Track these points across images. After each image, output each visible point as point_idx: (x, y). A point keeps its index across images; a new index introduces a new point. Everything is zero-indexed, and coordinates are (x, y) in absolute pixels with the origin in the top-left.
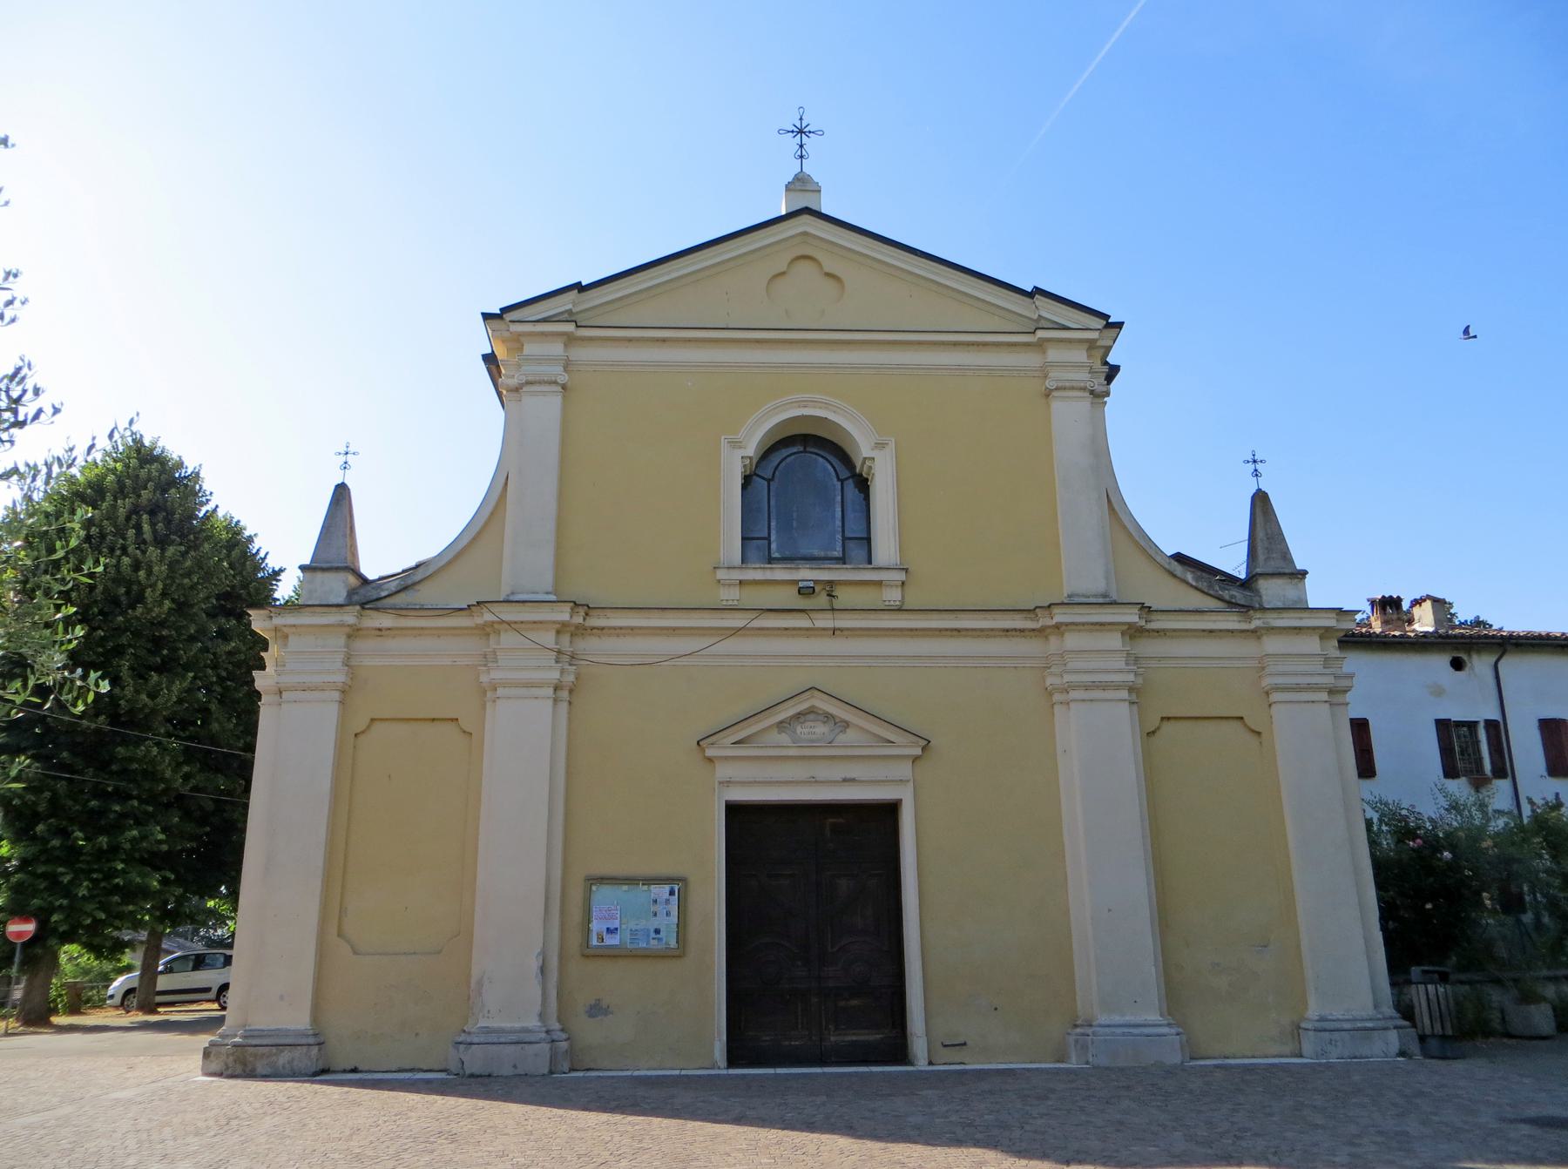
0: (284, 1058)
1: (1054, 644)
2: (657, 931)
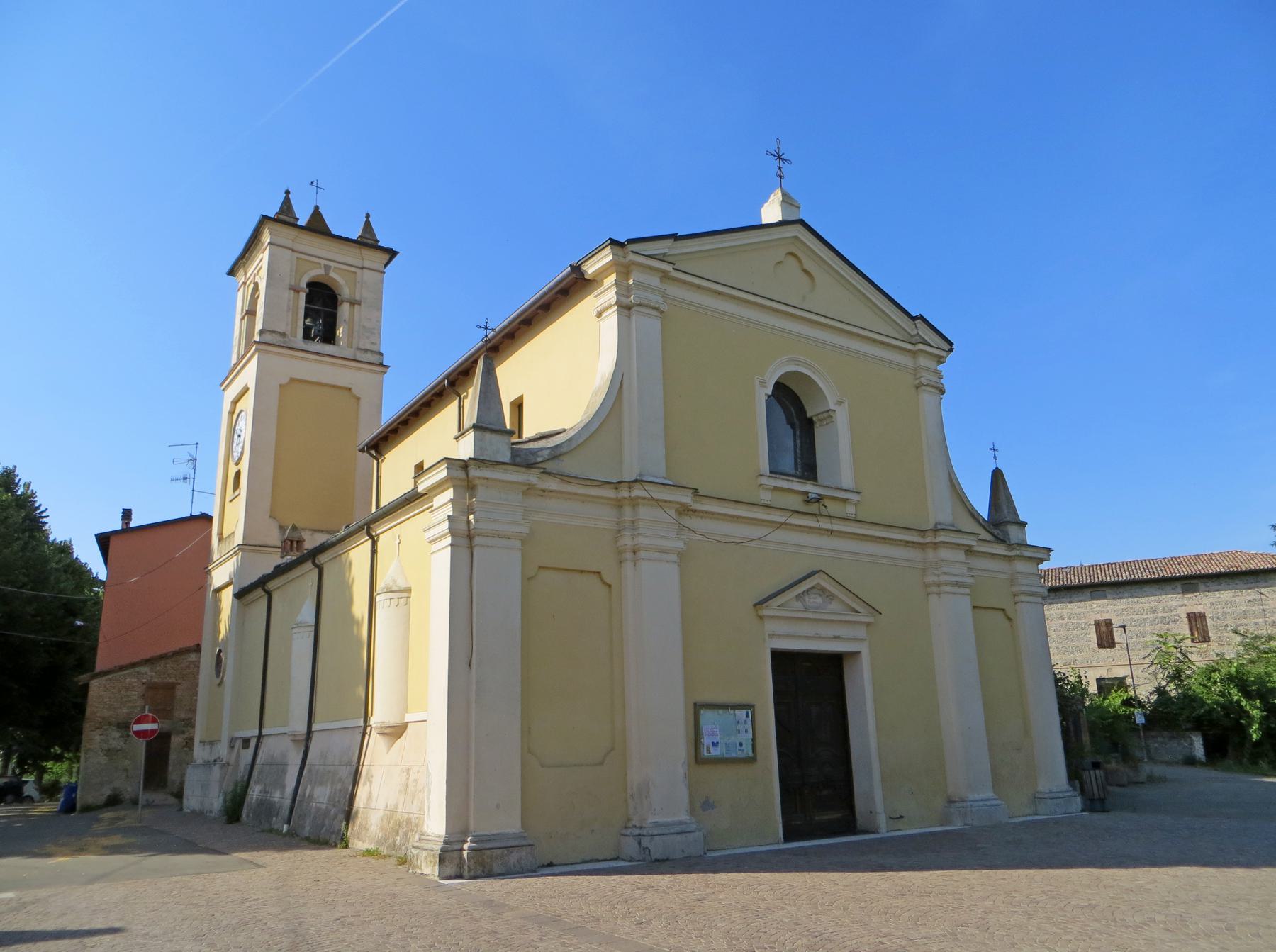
0: (513, 858)
1: (931, 554)
2: (741, 744)
